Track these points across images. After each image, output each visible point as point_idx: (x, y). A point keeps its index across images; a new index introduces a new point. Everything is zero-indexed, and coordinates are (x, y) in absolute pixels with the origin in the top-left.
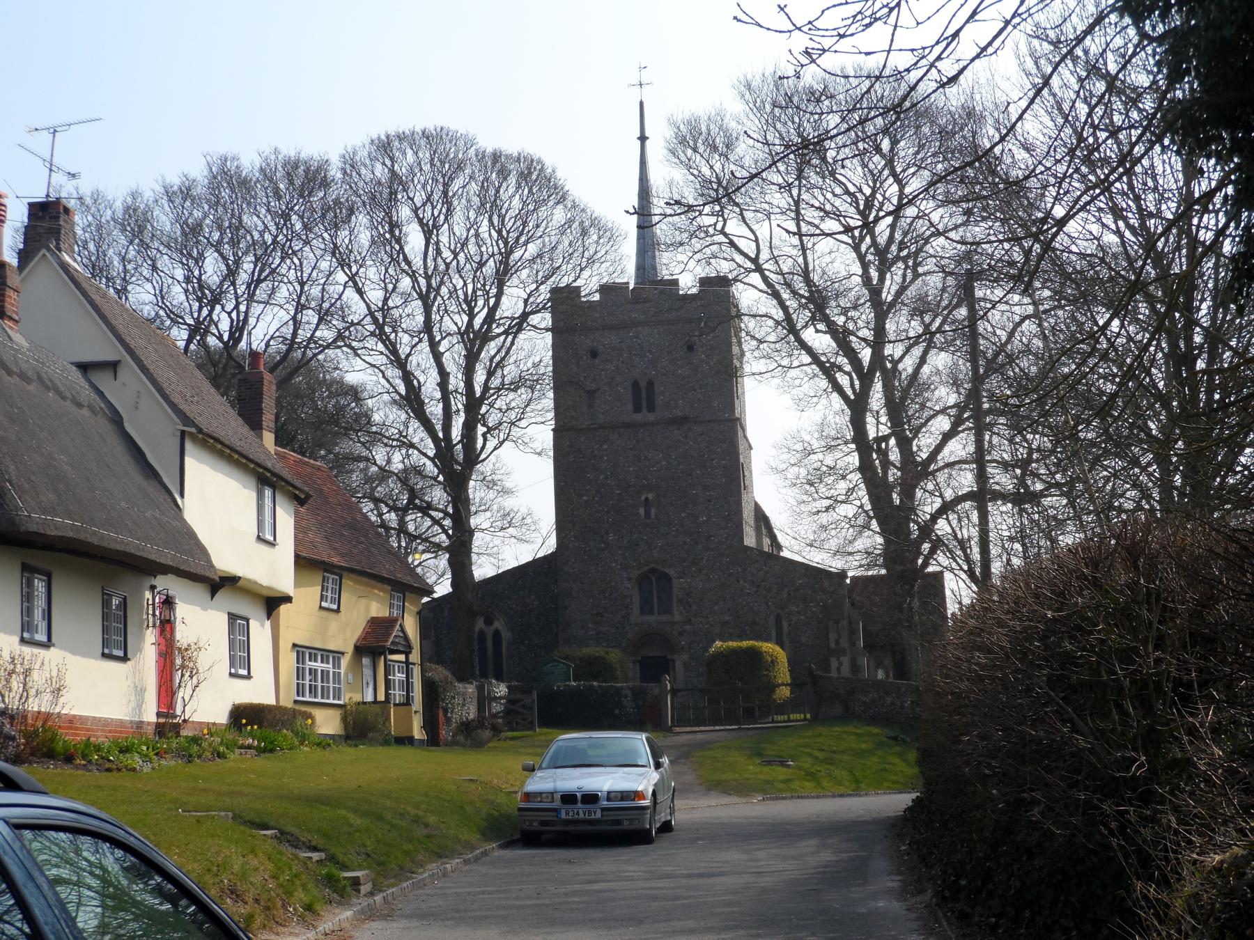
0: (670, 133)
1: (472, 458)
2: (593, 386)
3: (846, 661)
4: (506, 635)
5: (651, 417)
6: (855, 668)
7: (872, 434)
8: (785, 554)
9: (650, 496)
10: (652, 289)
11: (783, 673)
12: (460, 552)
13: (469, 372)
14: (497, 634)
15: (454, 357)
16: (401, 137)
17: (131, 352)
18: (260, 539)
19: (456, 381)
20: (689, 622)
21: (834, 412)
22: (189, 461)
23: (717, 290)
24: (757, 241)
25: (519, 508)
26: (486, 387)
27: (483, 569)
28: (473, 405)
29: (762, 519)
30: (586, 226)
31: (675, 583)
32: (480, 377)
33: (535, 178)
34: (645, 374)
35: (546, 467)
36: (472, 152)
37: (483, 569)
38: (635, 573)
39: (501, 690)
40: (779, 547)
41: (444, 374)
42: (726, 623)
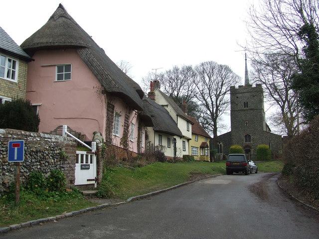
1: (217, 116)
4: (222, 145)
5: (247, 108)
15: (214, 99)
19: (214, 103)
25: (225, 124)
26: (219, 104)
27: (219, 134)
29: (267, 126)
32: (218, 102)
34: (246, 101)
35: (229, 117)
37: (219, 134)
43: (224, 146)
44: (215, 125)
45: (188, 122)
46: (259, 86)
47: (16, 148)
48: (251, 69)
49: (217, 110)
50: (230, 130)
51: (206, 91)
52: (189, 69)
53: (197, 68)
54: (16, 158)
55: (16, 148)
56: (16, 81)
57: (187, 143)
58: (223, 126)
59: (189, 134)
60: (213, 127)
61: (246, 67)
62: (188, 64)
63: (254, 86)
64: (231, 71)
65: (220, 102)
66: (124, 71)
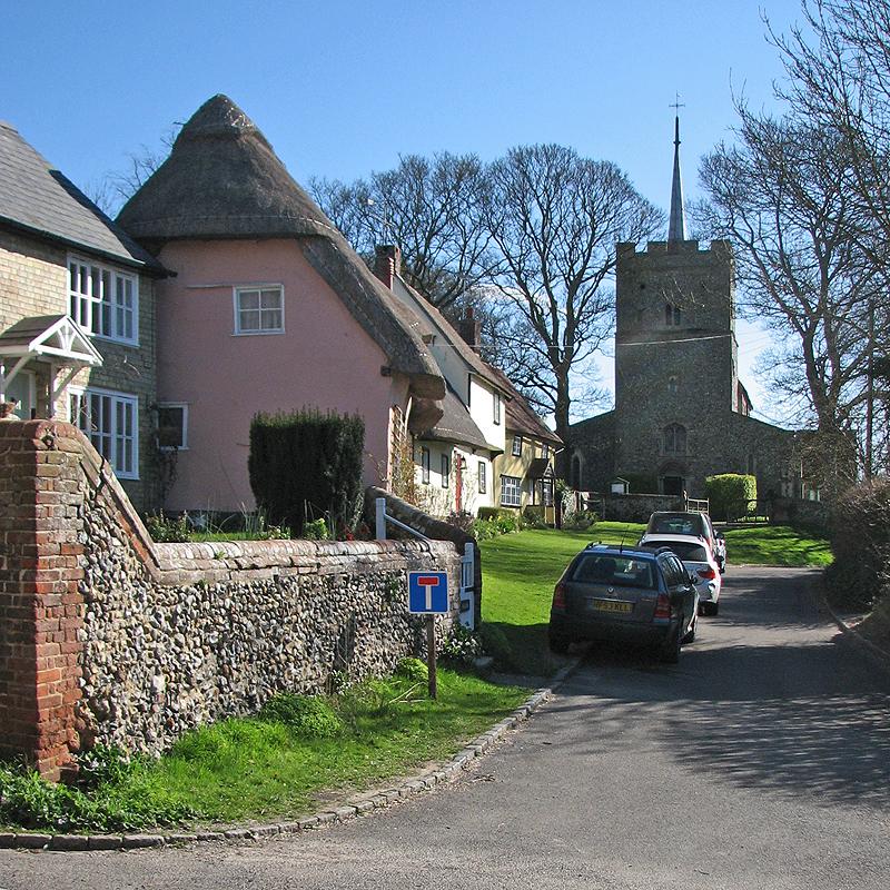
0: (700, 165)
1: (570, 354)
2: (642, 307)
3: (791, 485)
4: (582, 460)
5: (677, 328)
6: (797, 490)
7: (816, 355)
8: (753, 414)
9: (675, 378)
10: (677, 245)
11: (753, 494)
12: (562, 408)
13: (570, 306)
14: (577, 460)
15: (560, 290)
16: (530, 153)
17: (442, 332)
18: (495, 422)
19: (562, 309)
20: (695, 457)
21: (795, 342)
22: (472, 383)
23: (722, 249)
24: (752, 232)
25: (594, 383)
26: (580, 312)
27: (573, 420)
28: (573, 323)
29: (742, 392)
30: (648, 212)
31: (688, 432)
32: (576, 305)
33: (612, 179)
34: (673, 294)
35: (613, 361)
36: (573, 165)
37: (573, 420)
38: (664, 426)
39: (585, 495)
40: (749, 406)
41: (554, 303)
42: (719, 458)
43: (589, 464)
44: (563, 390)
45: (497, 392)
46: (722, 249)
47: (428, 588)
48: (695, 191)
49: (569, 333)
50: (610, 406)
51: (534, 261)
52: (467, 169)
53: (498, 168)
54: (429, 606)
55: (428, 588)
56: (135, 342)
57: (489, 465)
58: (593, 395)
59: (496, 437)
60: (555, 394)
61: (676, 170)
62: (460, 152)
63: (704, 245)
64: (628, 192)
65: (583, 304)
66: (179, 130)
